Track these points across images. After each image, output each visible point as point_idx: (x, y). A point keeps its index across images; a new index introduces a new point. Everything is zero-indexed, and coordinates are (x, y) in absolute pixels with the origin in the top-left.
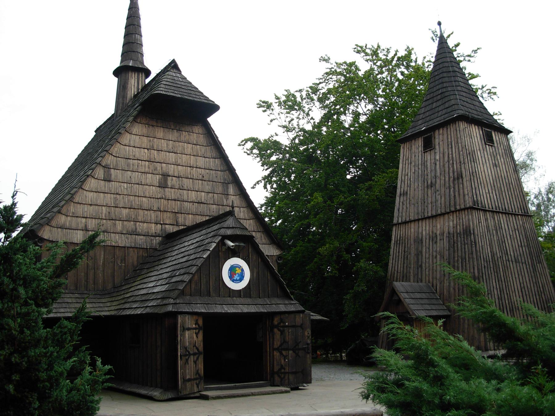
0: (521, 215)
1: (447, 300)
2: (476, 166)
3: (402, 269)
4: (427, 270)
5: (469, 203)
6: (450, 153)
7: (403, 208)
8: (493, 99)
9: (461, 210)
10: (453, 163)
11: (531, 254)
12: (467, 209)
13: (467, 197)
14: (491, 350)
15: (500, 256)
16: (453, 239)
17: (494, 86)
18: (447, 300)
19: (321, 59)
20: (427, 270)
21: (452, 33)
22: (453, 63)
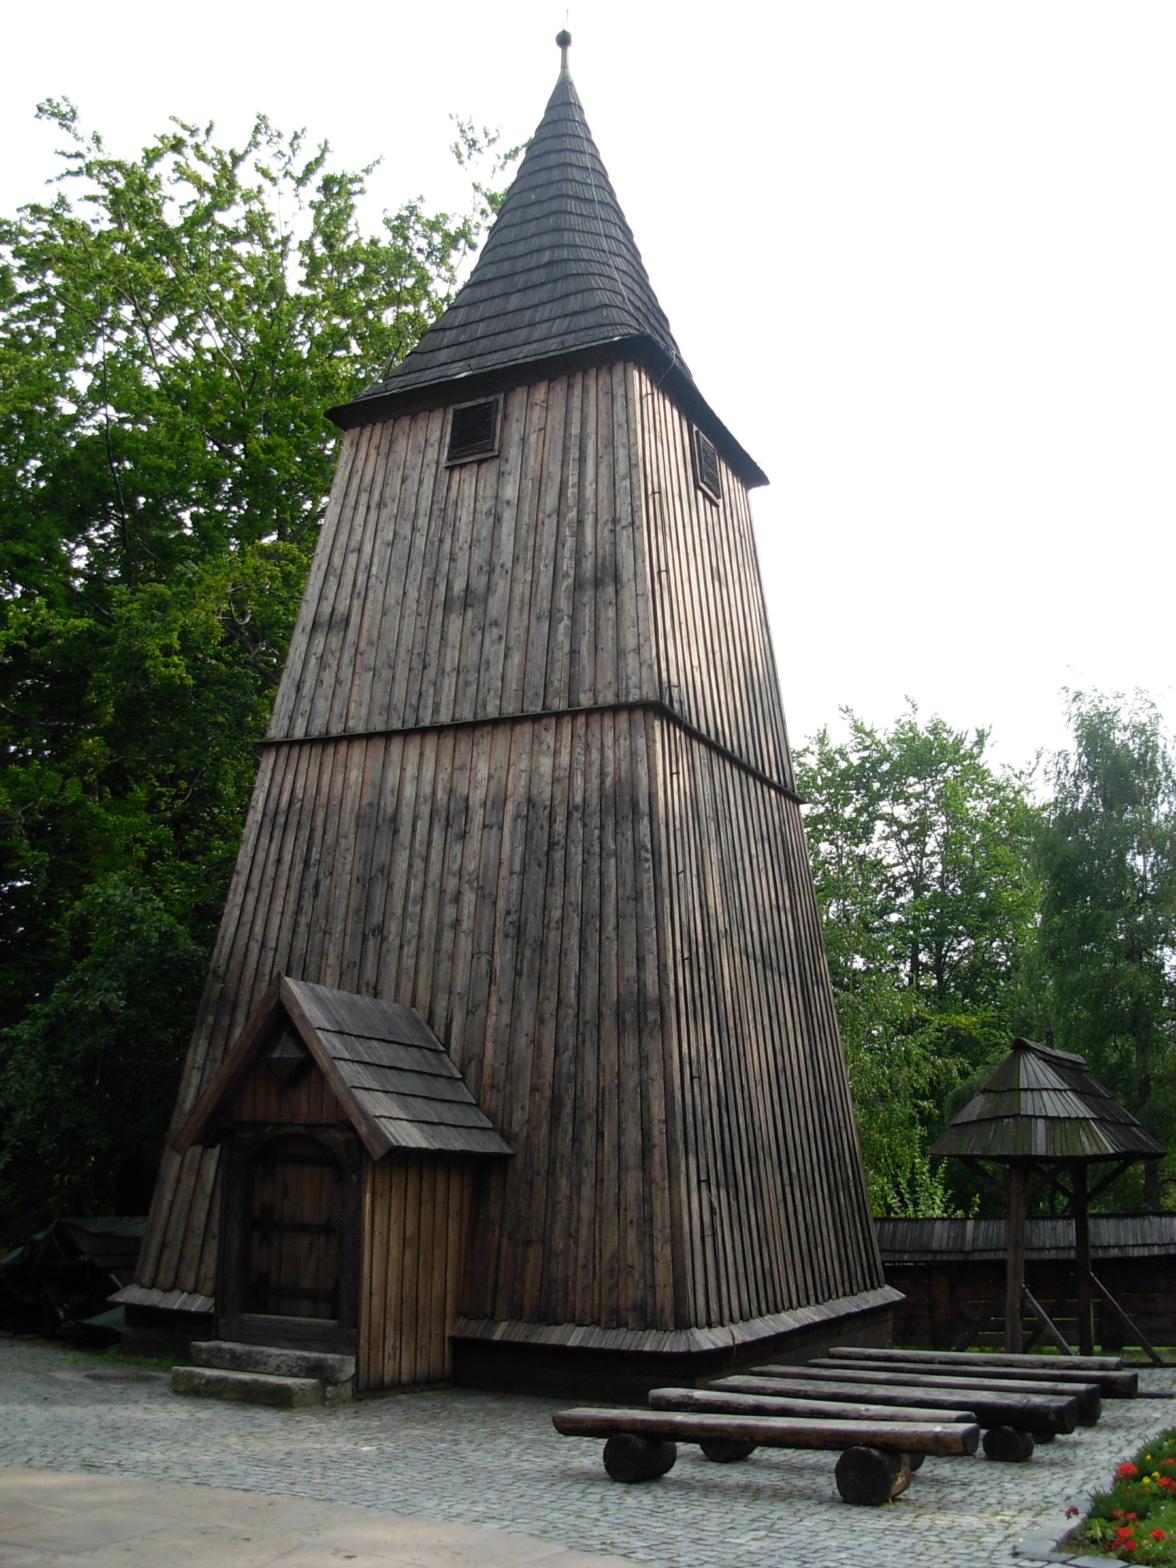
4: (409, 950)
19: (46, 107)
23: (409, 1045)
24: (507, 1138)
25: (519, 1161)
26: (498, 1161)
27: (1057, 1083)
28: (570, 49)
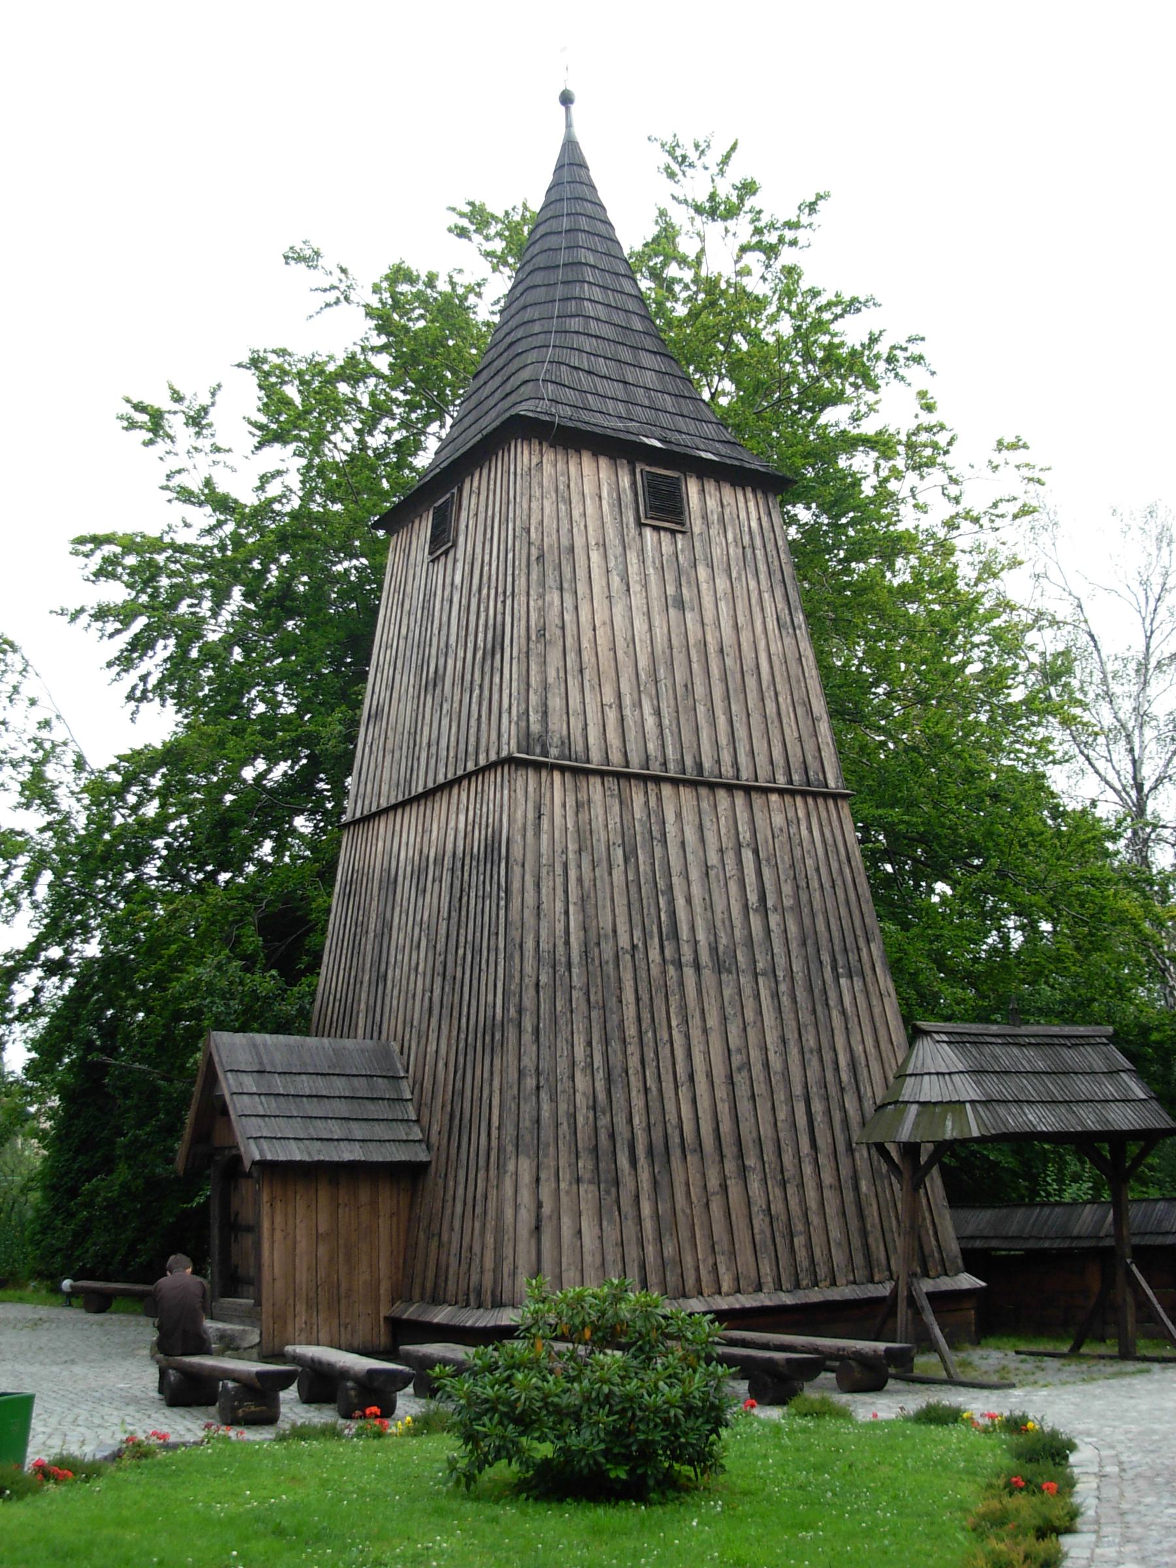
0: (781, 792)
8: (903, 379)
11: (809, 942)
15: (634, 947)
17: (914, 334)
19: (291, 255)
21: (733, 148)
27: (1128, 1065)
28: (573, 107)
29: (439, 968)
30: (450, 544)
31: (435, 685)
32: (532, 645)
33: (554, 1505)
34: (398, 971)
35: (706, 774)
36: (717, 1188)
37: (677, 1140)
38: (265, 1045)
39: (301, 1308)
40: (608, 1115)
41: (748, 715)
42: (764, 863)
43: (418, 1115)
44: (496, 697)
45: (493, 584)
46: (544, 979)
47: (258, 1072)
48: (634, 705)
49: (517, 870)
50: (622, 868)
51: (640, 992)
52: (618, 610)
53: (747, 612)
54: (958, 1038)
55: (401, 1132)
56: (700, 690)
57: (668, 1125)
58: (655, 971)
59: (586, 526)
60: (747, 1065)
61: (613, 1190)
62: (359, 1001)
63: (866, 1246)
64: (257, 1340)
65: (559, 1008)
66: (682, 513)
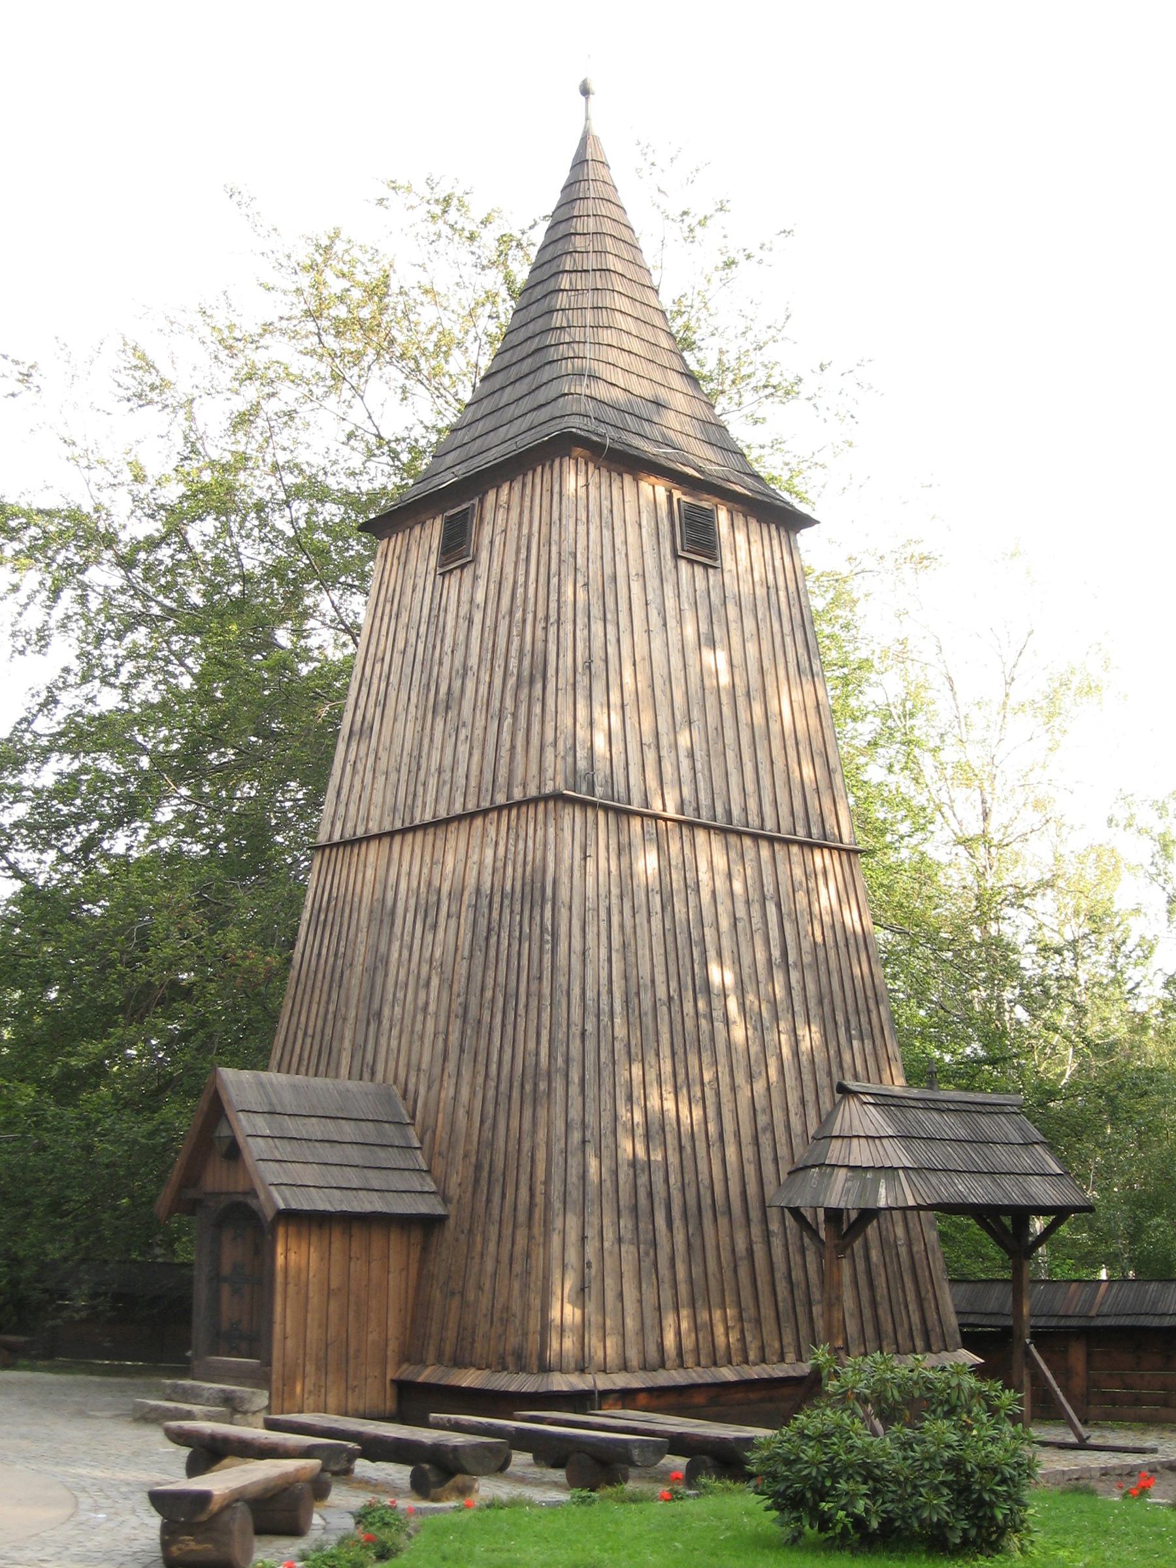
0: (801, 844)
1: (440, 1154)
2: (611, 636)
3: (320, 1023)
4: (395, 1032)
5: (554, 779)
6: (521, 579)
7: (352, 786)
9: (527, 802)
10: (524, 621)
11: (826, 1001)
12: (546, 799)
13: (549, 753)
14: (561, 1371)
15: (670, 998)
16: (486, 915)
18: (440, 1154)
20: (395, 1032)
22: (608, 240)
23: (338, 1118)
24: (446, 1200)
25: (451, 1222)
26: (429, 1224)
27: (1041, 1138)
29: (457, 1008)
30: (469, 559)
31: (448, 708)
32: (578, 677)
33: (810, 1558)
34: (398, 1009)
35: (735, 822)
36: (744, 1253)
37: (709, 1201)
38: (271, 1084)
39: (310, 1368)
40: (647, 1173)
41: (772, 763)
42: (785, 916)
43: (430, 1164)
44: (536, 728)
45: (531, 607)
46: (590, 1027)
47: (269, 1113)
48: (670, 746)
49: (564, 912)
50: (660, 916)
51: (676, 1046)
52: (657, 643)
53: (771, 657)
54: (882, 1100)
55: (415, 1183)
56: (729, 734)
57: (701, 1186)
58: (689, 1024)
59: (627, 555)
60: (771, 1125)
61: (652, 1253)
62: (342, 1038)
63: (876, 1316)
64: (266, 1403)
65: (603, 1060)
66: (715, 548)
